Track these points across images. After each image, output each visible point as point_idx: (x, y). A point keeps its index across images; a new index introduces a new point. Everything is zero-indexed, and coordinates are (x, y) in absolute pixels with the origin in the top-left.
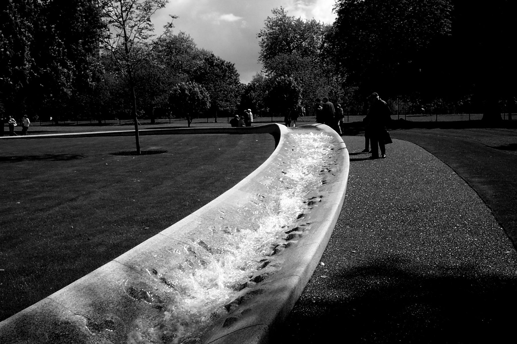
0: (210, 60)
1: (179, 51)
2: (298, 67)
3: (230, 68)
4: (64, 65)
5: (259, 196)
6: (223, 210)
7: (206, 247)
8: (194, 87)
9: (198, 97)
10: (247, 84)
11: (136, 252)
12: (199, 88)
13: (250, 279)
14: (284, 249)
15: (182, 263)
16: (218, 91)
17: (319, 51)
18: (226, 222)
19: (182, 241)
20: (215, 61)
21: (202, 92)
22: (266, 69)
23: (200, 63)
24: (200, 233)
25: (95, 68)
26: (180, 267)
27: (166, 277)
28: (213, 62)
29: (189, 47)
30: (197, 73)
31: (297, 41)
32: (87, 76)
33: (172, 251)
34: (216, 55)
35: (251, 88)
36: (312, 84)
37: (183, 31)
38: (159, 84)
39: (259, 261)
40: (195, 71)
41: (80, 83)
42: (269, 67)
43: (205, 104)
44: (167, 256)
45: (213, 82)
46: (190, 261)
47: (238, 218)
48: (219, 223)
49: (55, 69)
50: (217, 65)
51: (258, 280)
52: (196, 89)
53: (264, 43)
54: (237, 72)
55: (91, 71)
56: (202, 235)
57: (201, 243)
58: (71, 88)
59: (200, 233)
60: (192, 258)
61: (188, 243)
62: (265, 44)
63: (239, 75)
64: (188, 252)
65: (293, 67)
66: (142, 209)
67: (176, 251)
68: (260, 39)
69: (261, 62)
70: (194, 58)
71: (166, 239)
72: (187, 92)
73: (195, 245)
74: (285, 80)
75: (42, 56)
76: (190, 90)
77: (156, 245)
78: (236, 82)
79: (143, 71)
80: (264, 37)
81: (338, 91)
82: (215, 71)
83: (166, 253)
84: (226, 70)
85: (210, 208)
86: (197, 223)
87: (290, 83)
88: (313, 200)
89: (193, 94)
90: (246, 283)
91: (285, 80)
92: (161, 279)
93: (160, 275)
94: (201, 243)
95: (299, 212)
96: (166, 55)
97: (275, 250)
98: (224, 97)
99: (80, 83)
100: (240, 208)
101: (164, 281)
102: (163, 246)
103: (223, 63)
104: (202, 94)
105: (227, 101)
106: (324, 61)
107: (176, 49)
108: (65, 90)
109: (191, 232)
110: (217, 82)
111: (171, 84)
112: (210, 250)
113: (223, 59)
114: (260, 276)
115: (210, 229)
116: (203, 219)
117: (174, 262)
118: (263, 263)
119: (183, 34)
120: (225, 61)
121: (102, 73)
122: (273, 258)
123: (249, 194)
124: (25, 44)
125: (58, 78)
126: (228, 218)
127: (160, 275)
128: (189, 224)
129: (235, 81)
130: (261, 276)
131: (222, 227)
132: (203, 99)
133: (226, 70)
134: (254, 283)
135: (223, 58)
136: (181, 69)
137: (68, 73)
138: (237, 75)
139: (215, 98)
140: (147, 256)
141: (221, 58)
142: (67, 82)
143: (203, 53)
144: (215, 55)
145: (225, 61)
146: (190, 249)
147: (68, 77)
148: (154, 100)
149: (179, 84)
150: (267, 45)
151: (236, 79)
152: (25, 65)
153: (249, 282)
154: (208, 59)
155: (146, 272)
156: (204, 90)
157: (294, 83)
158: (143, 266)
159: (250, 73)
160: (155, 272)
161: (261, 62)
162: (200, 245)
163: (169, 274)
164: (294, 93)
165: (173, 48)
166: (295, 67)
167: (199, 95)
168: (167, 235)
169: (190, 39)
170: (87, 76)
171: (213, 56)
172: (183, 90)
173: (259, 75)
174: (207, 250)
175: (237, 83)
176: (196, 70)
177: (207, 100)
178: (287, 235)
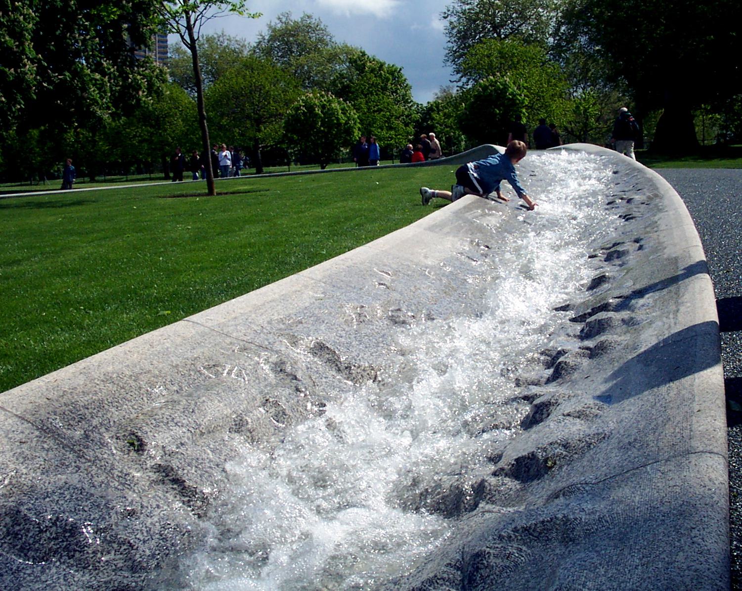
0: (359, 62)
1: (303, 49)
2: (518, 62)
3: (395, 74)
4: (98, 68)
5: (478, 244)
6: (386, 269)
7: (333, 361)
8: (329, 101)
9: (338, 119)
10: (425, 105)
11: (84, 372)
12: (339, 103)
13: (492, 468)
14: (586, 362)
15: (247, 411)
16: (374, 111)
17: (551, 40)
18: (395, 295)
19: (258, 341)
20: (368, 64)
21: (344, 111)
22: (459, 75)
23: (342, 67)
24: (319, 320)
25: (153, 72)
26: (239, 426)
27: (175, 463)
28: (364, 65)
29: (321, 40)
30: (337, 86)
31: (512, 23)
32: (138, 88)
33: (217, 374)
34: (370, 53)
35: (429, 112)
36: (542, 92)
37: (309, 13)
38: (269, 103)
39: (499, 399)
40: (333, 83)
41: (125, 100)
42: (464, 71)
43: (349, 131)
44: (197, 388)
45: (365, 96)
46: (276, 404)
47: (428, 290)
48: (376, 298)
49: (77, 74)
50: (372, 71)
51: (527, 469)
52: (335, 105)
53: (453, 28)
54: (407, 82)
55: (144, 76)
56: (323, 327)
57: (320, 348)
58: (108, 108)
59: (319, 320)
60: (283, 394)
61: (277, 347)
62: (455, 30)
63: (411, 88)
64: (272, 375)
65: (507, 61)
66: (171, 273)
67: (229, 373)
68: (446, 23)
69: (449, 63)
70: (330, 60)
71: (203, 335)
72: (318, 111)
73: (301, 357)
74: (496, 82)
75: (59, 57)
76: (323, 107)
77: (166, 353)
78: (406, 100)
79: (241, 80)
80: (454, 19)
81: (589, 107)
82: (366, 80)
83: (198, 378)
84: (388, 80)
85: (350, 263)
86: (308, 297)
87: (506, 87)
88: (620, 248)
89: (329, 113)
90: (483, 481)
91: (496, 82)
92: (159, 468)
93: (154, 455)
94: (320, 348)
95: (587, 275)
96: (282, 57)
97: (557, 366)
98: (386, 122)
99: (125, 100)
100: (432, 268)
101: (170, 477)
102: (189, 355)
103: (382, 65)
104: (344, 113)
105: (390, 128)
106: (560, 57)
107: (299, 45)
108: (99, 112)
109: (289, 317)
110: (372, 94)
111: (287, 104)
112: (346, 370)
113: (382, 61)
114: (532, 457)
115: (348, 309)
116: (328, 287)
117: (215, 409)
118: (526, 409)
119: (309, 17)
120: (385, 63)
121: (164, 81)
122: (551, 388)
123: (451, 238)
124: (23, 29)
125: (84, 89)
126: (400, 287)
127: (154, 455)
128: (284, 298)
129: (403, 98)
130: (540, 455)
131: (385, 306)
132: (346, 123)
133: (388, 80)
134: (512, 484)
135: (381, 58)
136: (308, 79)
137: (102, 80)
138: (407, 88)
139: (370, 125)
140: (124, 387)
141: (377, 58)
142: (102, 98)
143: (348, 51)
144: (366, 53)
145: (385, 63)
146: (279, 368)
147: (101, 88)
148: (259, 131)
149: (303, 97)
150: (459, 32)
151: (404, 96)
152: (25, 65)
153: (493, 480)
154: (355, 61)
155: (103, 445)
156: (348, 106)
157: (513, 88)
158: (95, 422)
159: (431, 83)
160: (138, 445)
161: (449, 63)
162: (315, 354)
163: (190, 451)
164: (513, 105)
165: (293, 42)
166: (513, 63)
167: (341, 115)
168: (209, 324)
169: (322, 27)
170: (138, 88)
171: (364, 54)
172: (310, 108)
173: (445, 91)
174: (339, 370)
175: (406, 102)
176: (335, 80)
177: (355, 123)
178: (579, 327)
